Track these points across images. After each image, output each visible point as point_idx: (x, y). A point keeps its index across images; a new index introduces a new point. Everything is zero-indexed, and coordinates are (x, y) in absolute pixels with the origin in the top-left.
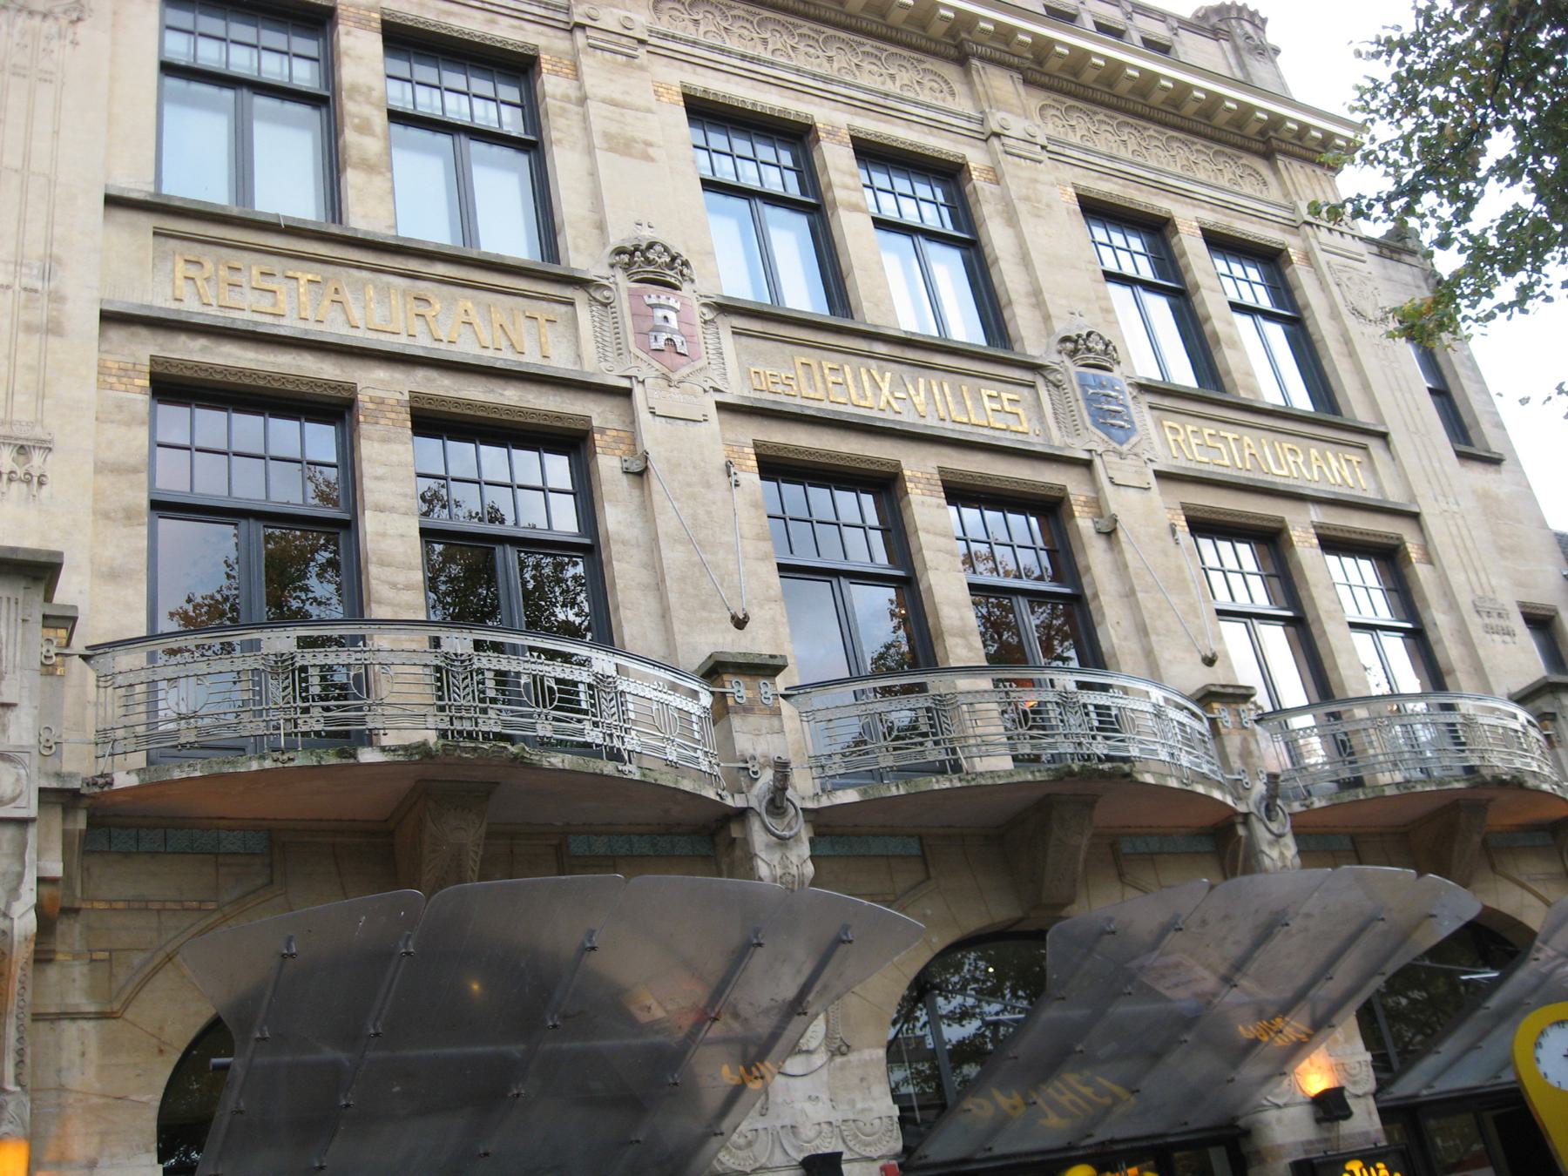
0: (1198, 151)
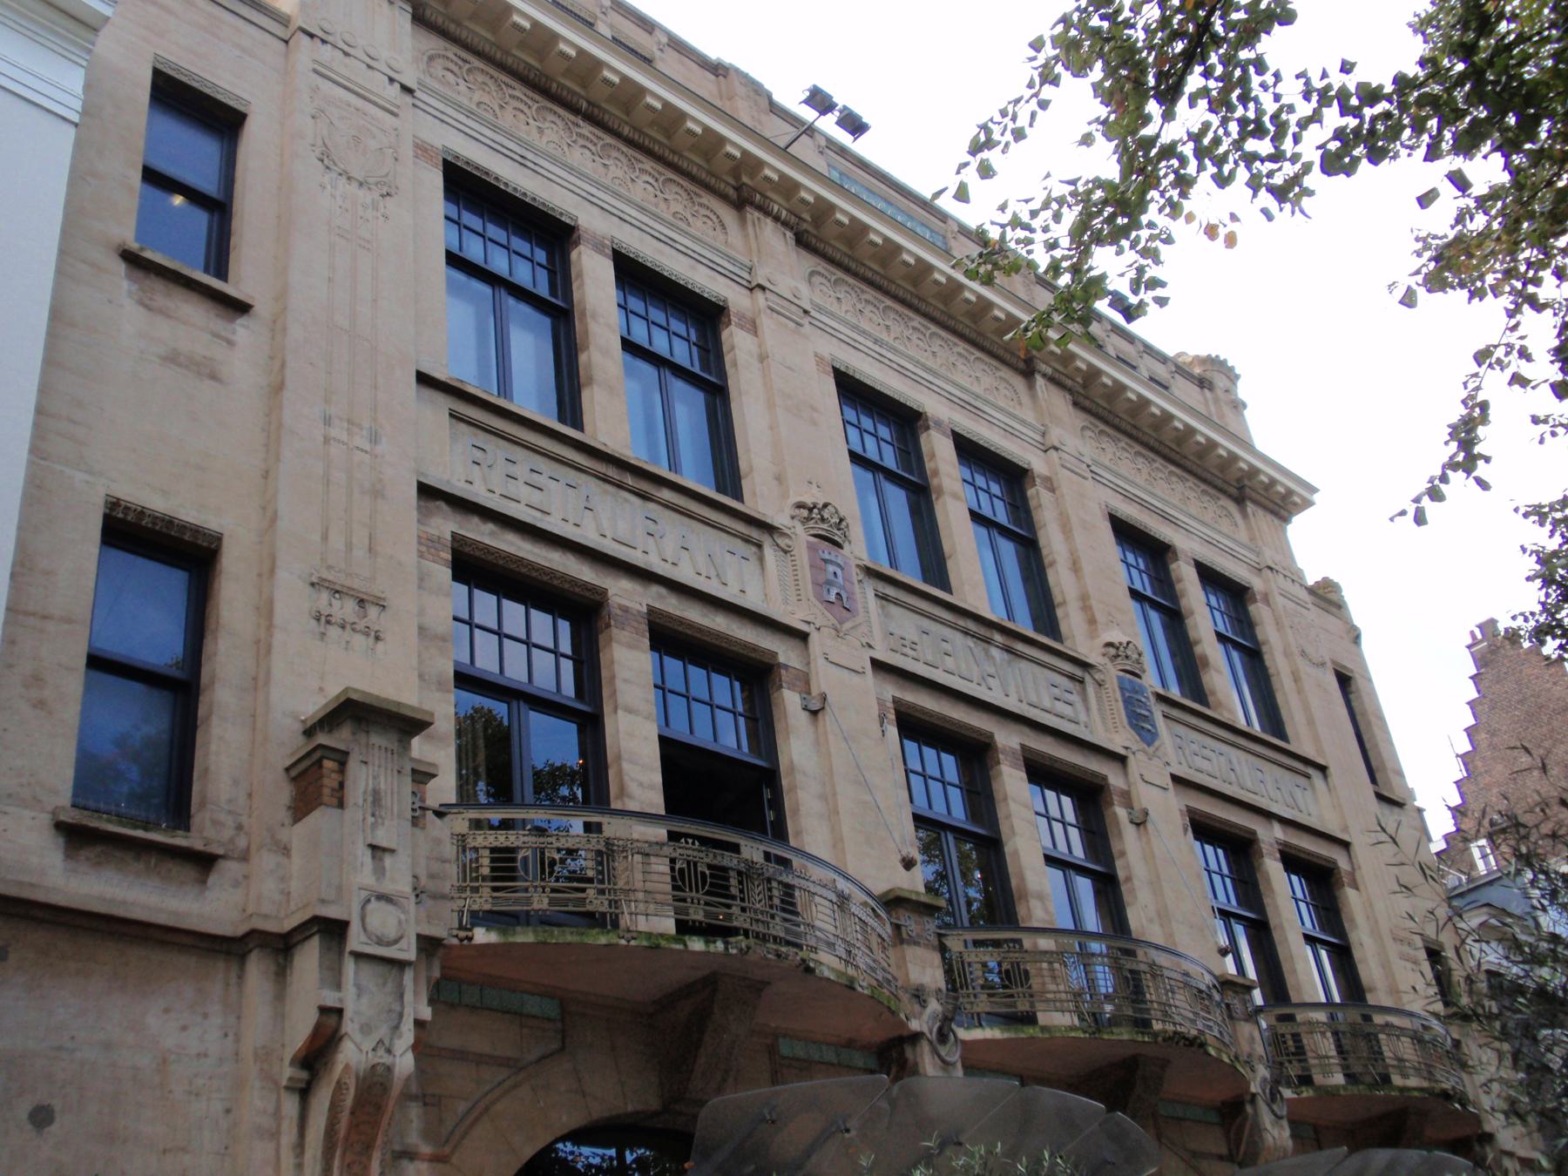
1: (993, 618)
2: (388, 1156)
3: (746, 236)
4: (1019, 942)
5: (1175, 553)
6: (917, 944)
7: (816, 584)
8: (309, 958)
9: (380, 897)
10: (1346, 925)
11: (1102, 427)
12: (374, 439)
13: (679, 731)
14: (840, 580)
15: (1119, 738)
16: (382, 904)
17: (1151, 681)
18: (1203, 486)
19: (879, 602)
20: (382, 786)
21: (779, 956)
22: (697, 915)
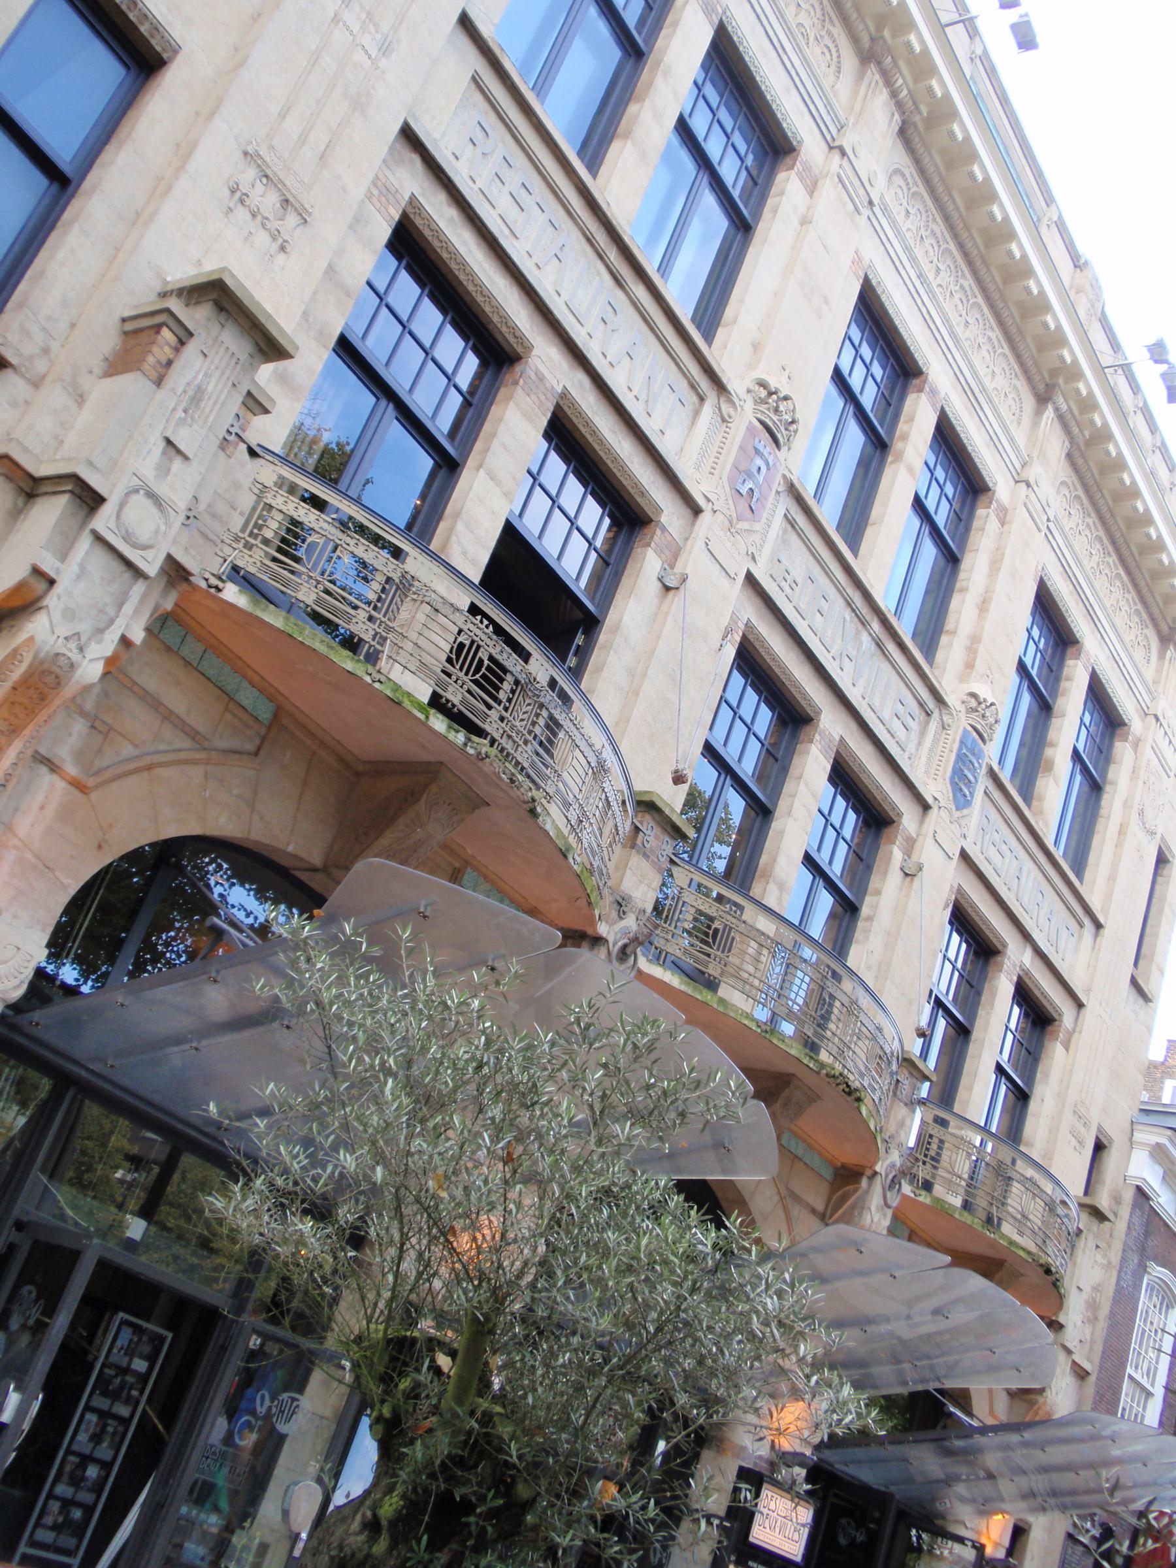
0: (933, 233)
1: (882, 605)
2: (29, 752)
3: (855, 93)
4: (741, 908)
5: (1079, 652)
6: (646, 856)
7: (735, 467)
8: (51, 511)
9: (151, 495)
10: (1038, 1075)
11: (1080, 492)
12: (386, 49)
13: (530, 527)
14: (761, 478)
15: (934, 787)
16: (148, 503)
17: (992, 751)
18: (1139, 607)
19: (785, 524)
20: (210, 388)
21: (512, 781)
22: (454, 696)
